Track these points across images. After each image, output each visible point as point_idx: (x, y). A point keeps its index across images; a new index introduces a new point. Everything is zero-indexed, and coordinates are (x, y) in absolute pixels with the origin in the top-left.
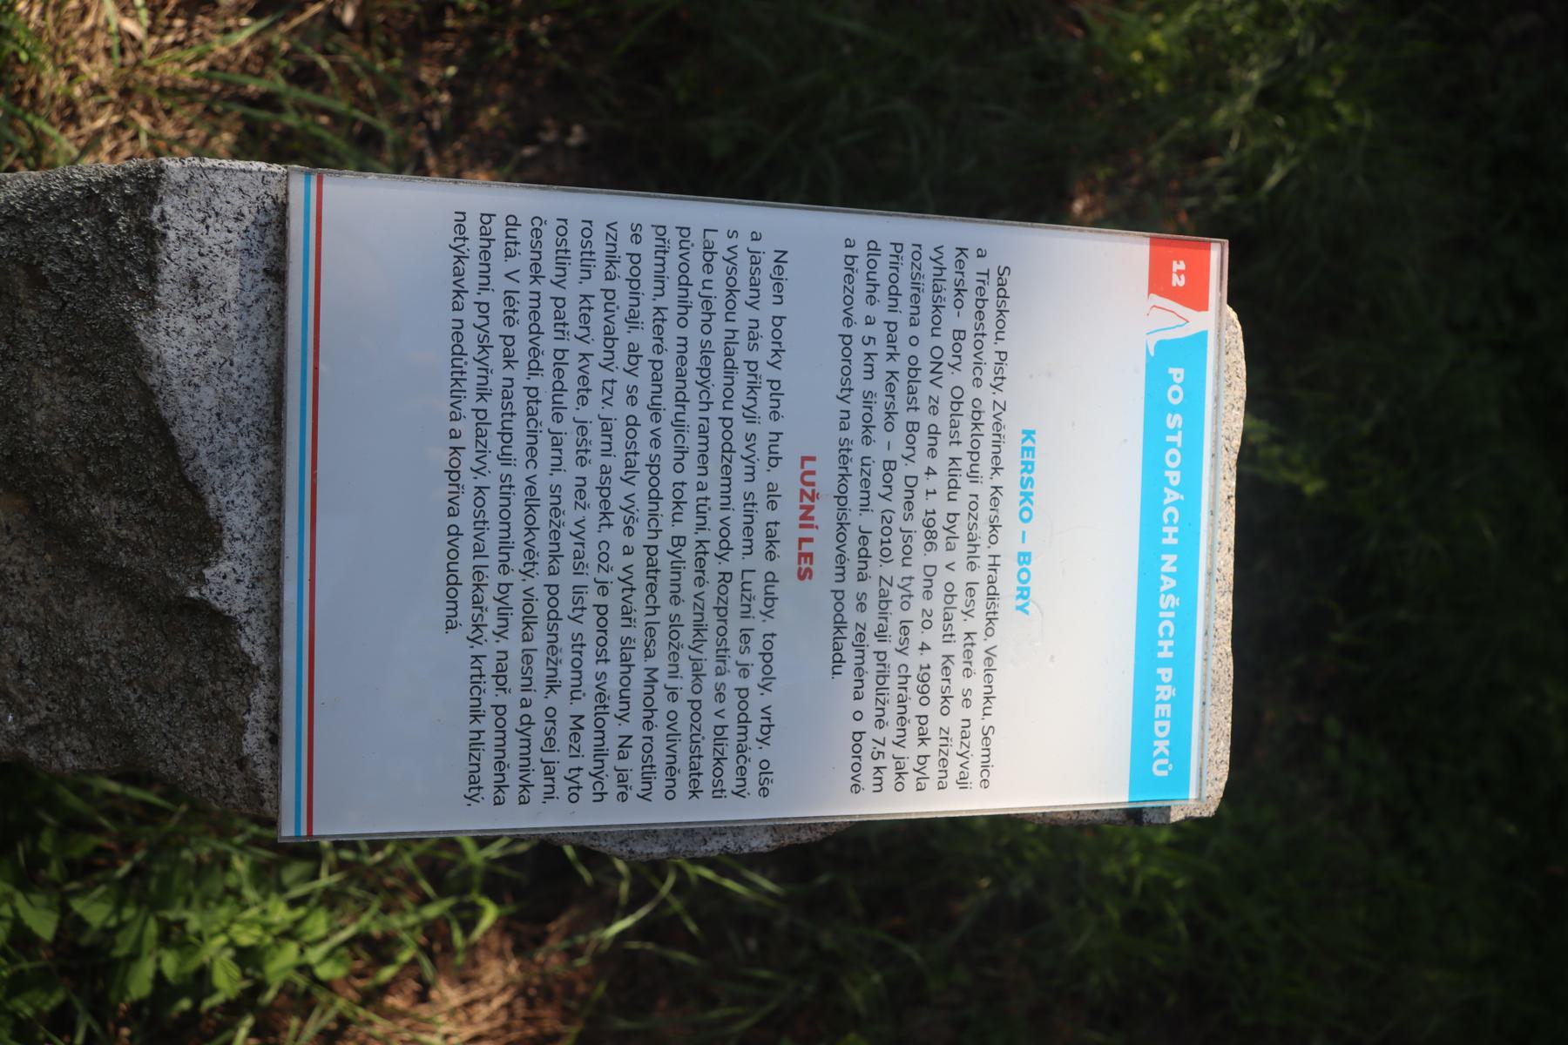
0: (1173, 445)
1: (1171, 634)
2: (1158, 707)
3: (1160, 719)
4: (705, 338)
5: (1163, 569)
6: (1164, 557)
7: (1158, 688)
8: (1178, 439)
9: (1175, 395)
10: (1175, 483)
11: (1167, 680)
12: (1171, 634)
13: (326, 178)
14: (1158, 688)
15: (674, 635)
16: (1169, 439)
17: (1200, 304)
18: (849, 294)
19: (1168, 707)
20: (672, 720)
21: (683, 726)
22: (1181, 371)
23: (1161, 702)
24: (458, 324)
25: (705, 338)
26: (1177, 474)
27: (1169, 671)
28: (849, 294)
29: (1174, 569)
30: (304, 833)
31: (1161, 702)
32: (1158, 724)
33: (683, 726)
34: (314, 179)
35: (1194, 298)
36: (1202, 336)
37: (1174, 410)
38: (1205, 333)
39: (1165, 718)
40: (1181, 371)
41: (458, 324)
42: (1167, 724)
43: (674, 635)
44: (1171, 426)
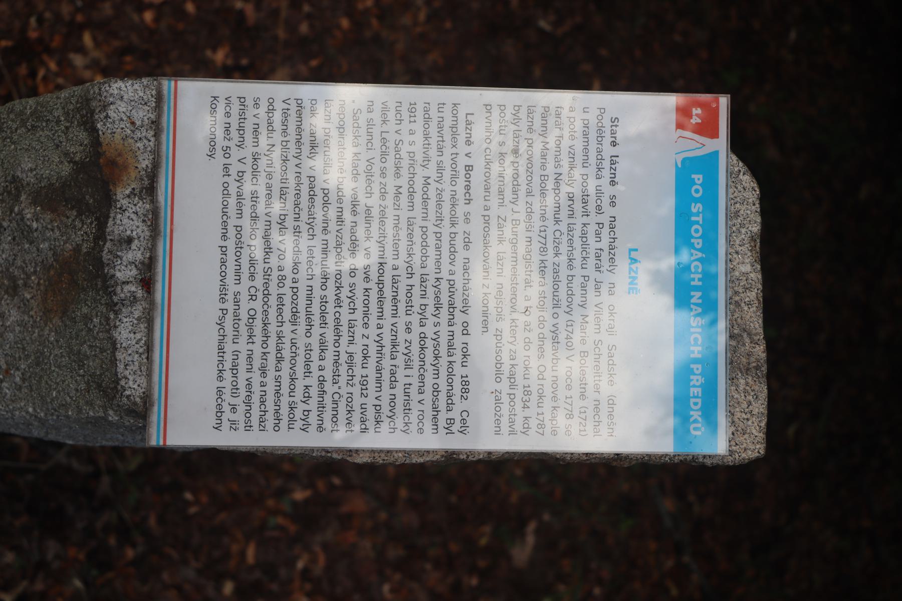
0: (697, 223)
1: (699, 343)
2: (692, 390)
3: (694, 397)
4: (383, 165)
5: (692, 301)
6: (692, 293)
7: (692, 377)
8: (700, 219)
9: (697, 191)
10: (699, 247)
11: (699, 372)
12: (699, 343)
13: (179, 82)
14: (692, 377)
15: (498, 409)
16: (693, 219)
17: (714, 134)
18: (223, 277)
19: (700, 390)
20: (280, 297)
21: (287, 300)
22: (701, 176)
23: (694, 386)
24: (250, 353)
25: (383, 165)
26: (700, 241)
27: (700, 366)
28: (223, 277)
29: (700, 301)
30: (161, 443)
31: (694, 386)
32: (692, 401)
33: (287, 300)
34: (173, 83)
35: (708, 129)
36: (716, 154)
37: (696, 201)
38: (716, 154)
39: (697, 397)
40: (701, 176)
41: (250, 353)
42: (699, 401)
43: (498, 409)
44: (694, 210)
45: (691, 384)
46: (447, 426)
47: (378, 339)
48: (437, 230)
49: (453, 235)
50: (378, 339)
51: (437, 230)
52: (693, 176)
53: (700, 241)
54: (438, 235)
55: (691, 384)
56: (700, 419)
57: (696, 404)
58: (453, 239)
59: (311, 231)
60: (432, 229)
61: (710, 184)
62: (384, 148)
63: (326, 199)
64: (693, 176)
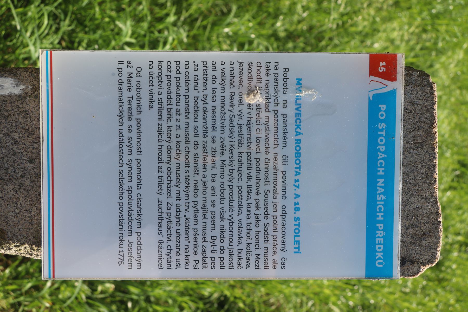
0: (382, 135)
2: (377, 239)
3: (379, 244)
5: (379, 184)
7: (377, 232)
8: (384, 133)
16: (379, 133)
22: (385, 106)
23: (379, 237)
26: (384, 147)
31: (379, 237)
32: (377, 246)
38: (393, 93)
39: (381, 244)
40: (385, 106)
42: (382, 246)
45: (377, 236)
46: (212, 241)
47: (129, 144)
48: (230, 184)
49: (240, 251)
50: (129, 144)
51: (230, 184)
52: (380, 106)
53: (384, 147)
54: (231, 187)
55: (377, 236)
56: (382, 257)
57: (379, 248)
58: (240, 253)
59: (121, 120)
60: (227, 183)
61: (391, 111)
62: (196, 108)
63: (222, 263)
64: (380, 106)
